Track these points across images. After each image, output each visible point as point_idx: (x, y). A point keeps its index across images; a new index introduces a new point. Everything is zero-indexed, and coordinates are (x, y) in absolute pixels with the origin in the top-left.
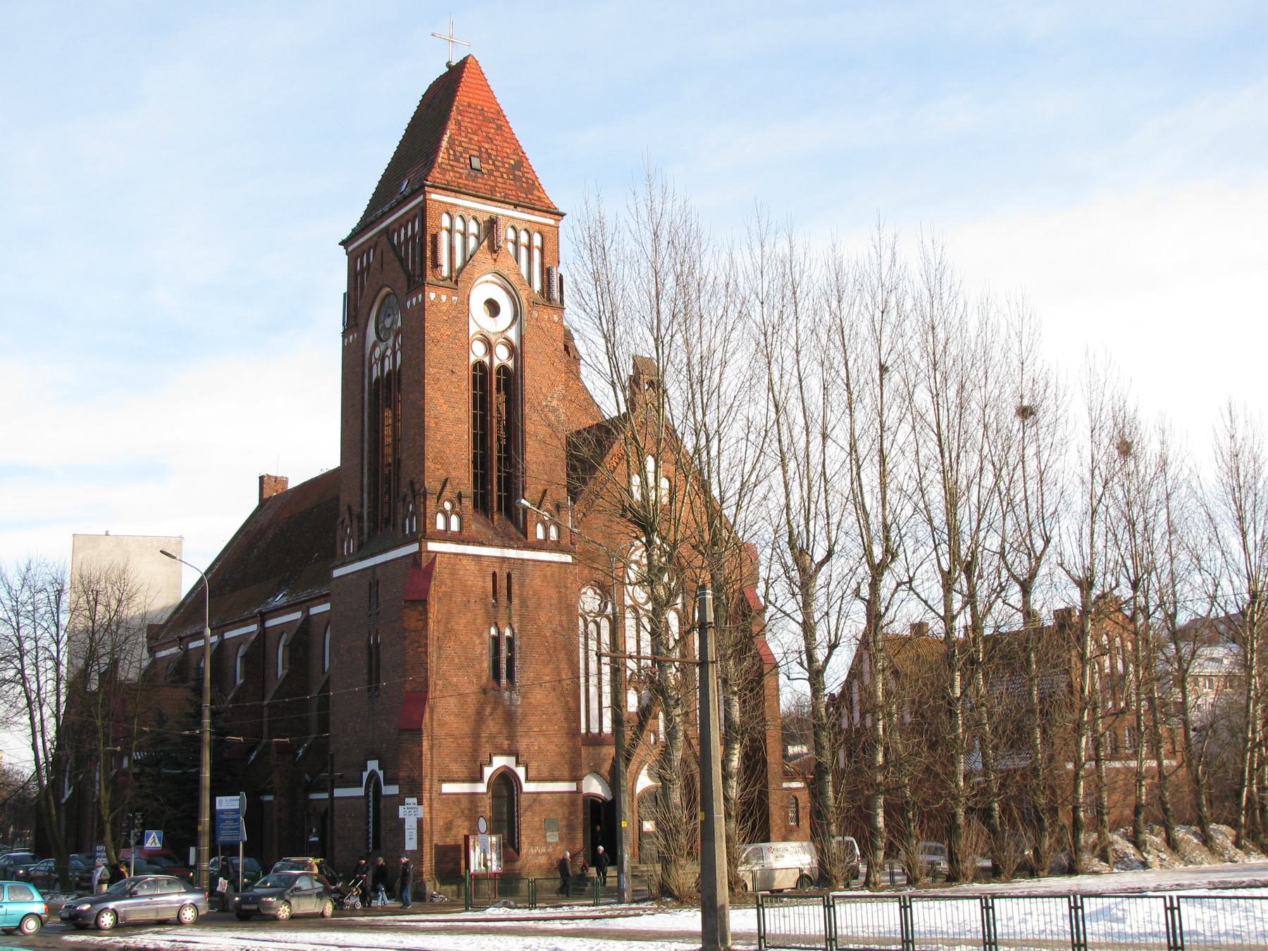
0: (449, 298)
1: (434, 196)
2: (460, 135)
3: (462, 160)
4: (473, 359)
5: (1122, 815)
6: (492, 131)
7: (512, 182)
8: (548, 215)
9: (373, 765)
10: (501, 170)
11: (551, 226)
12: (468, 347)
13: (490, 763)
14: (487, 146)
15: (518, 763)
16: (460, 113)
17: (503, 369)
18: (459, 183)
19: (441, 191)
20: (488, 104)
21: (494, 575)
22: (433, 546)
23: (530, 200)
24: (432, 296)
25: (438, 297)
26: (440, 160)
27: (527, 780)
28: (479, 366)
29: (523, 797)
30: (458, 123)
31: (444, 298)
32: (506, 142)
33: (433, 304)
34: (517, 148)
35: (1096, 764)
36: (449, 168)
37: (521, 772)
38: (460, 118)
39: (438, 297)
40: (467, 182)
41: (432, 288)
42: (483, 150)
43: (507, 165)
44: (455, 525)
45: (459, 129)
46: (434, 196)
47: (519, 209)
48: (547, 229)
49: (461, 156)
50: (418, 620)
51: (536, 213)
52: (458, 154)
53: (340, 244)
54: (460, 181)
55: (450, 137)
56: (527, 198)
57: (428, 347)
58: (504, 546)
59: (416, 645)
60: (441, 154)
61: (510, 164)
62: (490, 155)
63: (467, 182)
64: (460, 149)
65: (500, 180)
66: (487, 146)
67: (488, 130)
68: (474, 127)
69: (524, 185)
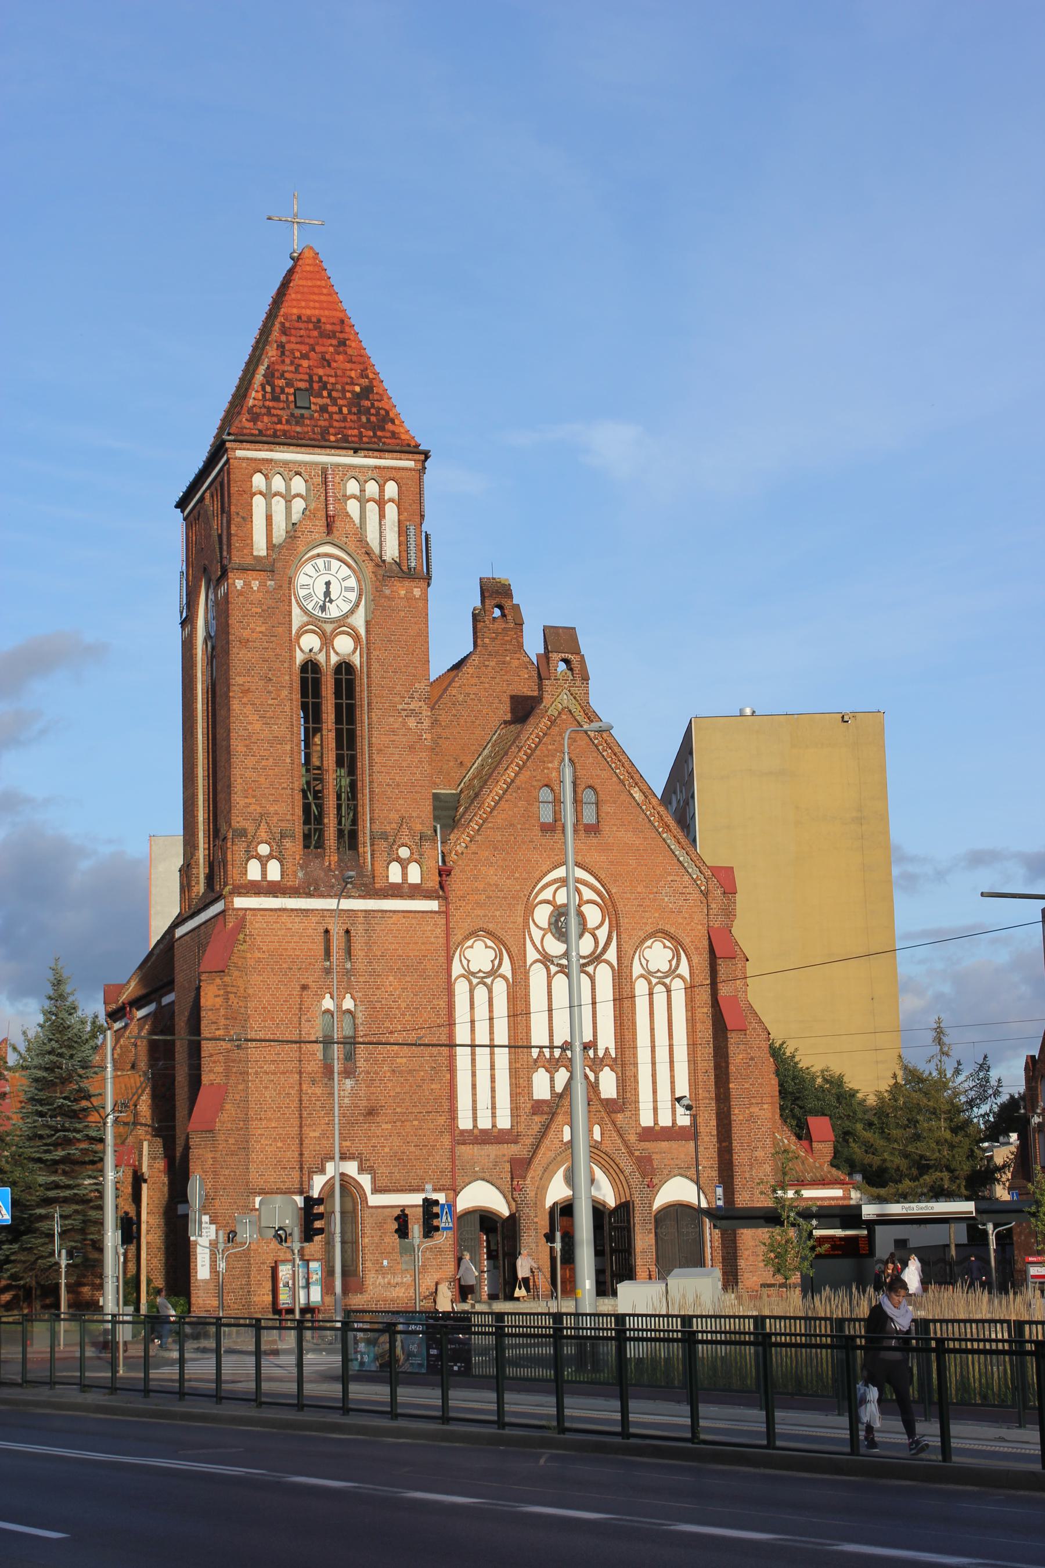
0: (263, 584)
1: (239, 453)
2: (283, 362)
3: (283, 397)
4: (299, 658)
5: (29, 1041)
6: (331, 349)
7: (354, 418)
8: (403, 456)
9: (351, 1168)
10: (340, 402)
11: (410, 469)
12: (292, 643)
13: (322, 1171)
14: (321, 372)
15: (361, 1170)
16: (284, 331)
17: (345, 668)
18: (276, 431)
19: (248, 445)
20: (327, 313)
21: (327, 931)
22: (240, 902)
23: (380, 438)
24: (239, 584)
25: (248, 584)
26: (251, 402)
27: (376, 1190)
28: (310, 668)
29: (369, 1222)
30: (281, 346)
31: (255, 585)
32: (350, 361)
33: (241, 593)
34: (364, 366)
35: (325, 1050)
36: (264, 411)
37: (365, 1181)
38: (284, 339)
39: (248, 584)
40: (287, 427)
41: (238, 574)
42: (315, 378)
43: (348, 395)
44: (274, 872)
45: (283, 353)
46: (239, 453)
47: (362, 453)
48: (404, 474)
49: (283, 392)
50: (216, 996)
51: (387, 455)
52: (278, 390)
53: (177, 507)
54: (279, 427)
55: (268, 368)
56: (375, 435)
57: (234, 651)
58: (339, 896)
59: (214, 1027)
60: (253, 394)
61: (353, 392)
62: (324, 387)
63: (287, 427)
64: (281, 382)
65: (336, 417)
66: (321, 372)
67: (323, 349)
68: (305, 349)
69: (373, 419)
